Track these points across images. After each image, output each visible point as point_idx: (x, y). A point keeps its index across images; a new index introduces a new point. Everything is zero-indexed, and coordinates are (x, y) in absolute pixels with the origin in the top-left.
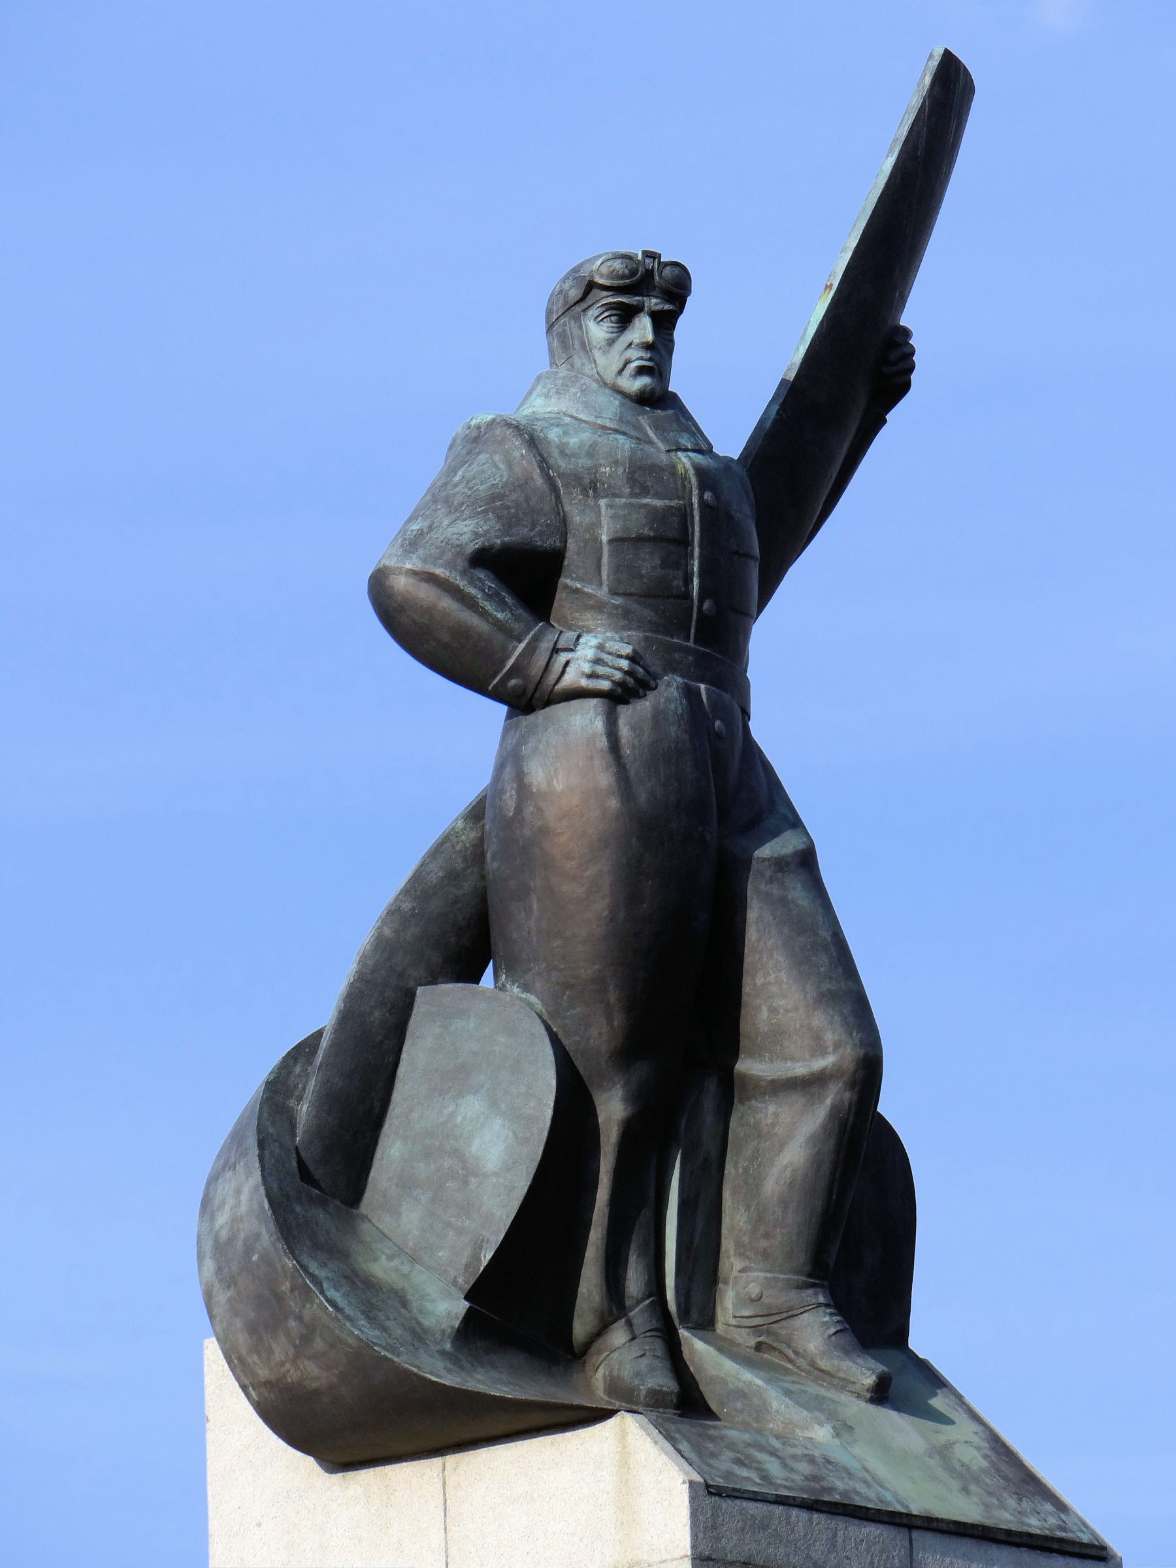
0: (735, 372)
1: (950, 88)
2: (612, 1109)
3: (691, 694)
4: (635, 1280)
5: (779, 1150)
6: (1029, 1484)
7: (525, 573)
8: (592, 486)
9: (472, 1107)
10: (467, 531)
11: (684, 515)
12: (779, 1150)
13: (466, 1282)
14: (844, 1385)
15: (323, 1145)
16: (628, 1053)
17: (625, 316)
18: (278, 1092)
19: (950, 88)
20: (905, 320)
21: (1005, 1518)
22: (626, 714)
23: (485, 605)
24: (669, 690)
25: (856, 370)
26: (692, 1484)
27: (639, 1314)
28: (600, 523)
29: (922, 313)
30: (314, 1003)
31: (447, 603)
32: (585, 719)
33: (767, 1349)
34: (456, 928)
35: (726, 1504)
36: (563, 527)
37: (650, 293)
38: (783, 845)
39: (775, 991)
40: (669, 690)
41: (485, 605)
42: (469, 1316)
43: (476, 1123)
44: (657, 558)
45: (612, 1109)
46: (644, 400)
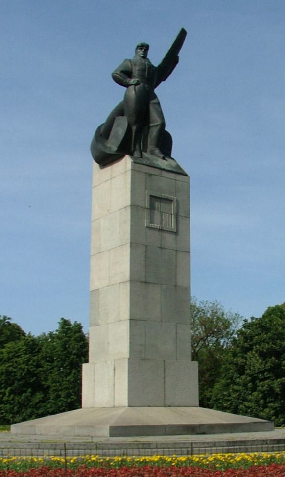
0: (156, 58)
1: (183, 35)
2: (134, 128)
3: (144, 86)
4: (137, 147)
5: (154, 132)
6: (180, 168)
7: (128, 73)
8: (135, 65)
9: (119, 128)
10: (121, 69)
11: (146, 68)
12: (154, 132)
13: (118, 145)
14: (159, 157)
15: (103, 133)
16: (136, 122)
17: (142, 49)
18: (99, 128)
19: (183, 35)
20: (179, 55)
21: (179, 171)
22: (137, 87)
23: (123, 77)
24: (142, 85)
25: (171, 60)
26: (132, 162)
27: (137, 151)
28: (136, 71)
29: (181, 54)
30: (103, 119)
31: (117, 76)
32: (132, 87)
33: (152, 153)
34: (120, 112)
35: (136, 164)
36: (132, 69)
37: (144, 48)
38: (154, 101)
39: (154, 115)
40: (142, 85)
41: (123, 77)
42: (117, 150)
43: (120, 130)
44: (146, 79)
45: (134, 128)
46: (143, 57)
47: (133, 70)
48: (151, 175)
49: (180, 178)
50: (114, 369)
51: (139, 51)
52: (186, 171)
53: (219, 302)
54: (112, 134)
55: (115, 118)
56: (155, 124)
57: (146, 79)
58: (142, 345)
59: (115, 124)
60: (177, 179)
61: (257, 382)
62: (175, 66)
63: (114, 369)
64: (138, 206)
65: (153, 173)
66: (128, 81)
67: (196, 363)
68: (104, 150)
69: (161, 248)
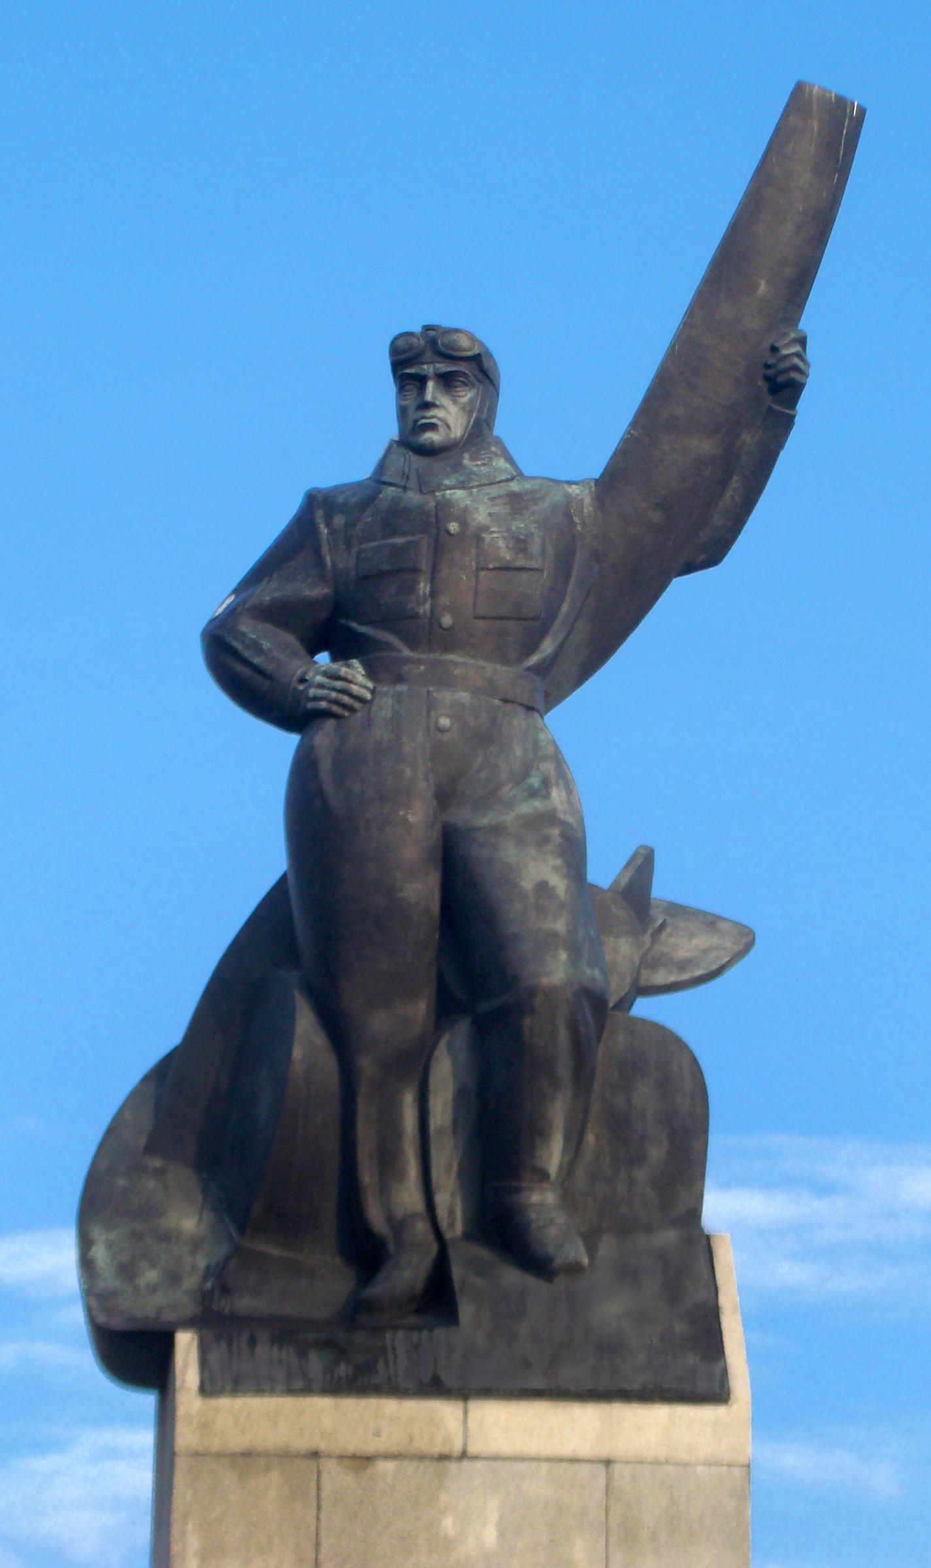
0: (564, 424)
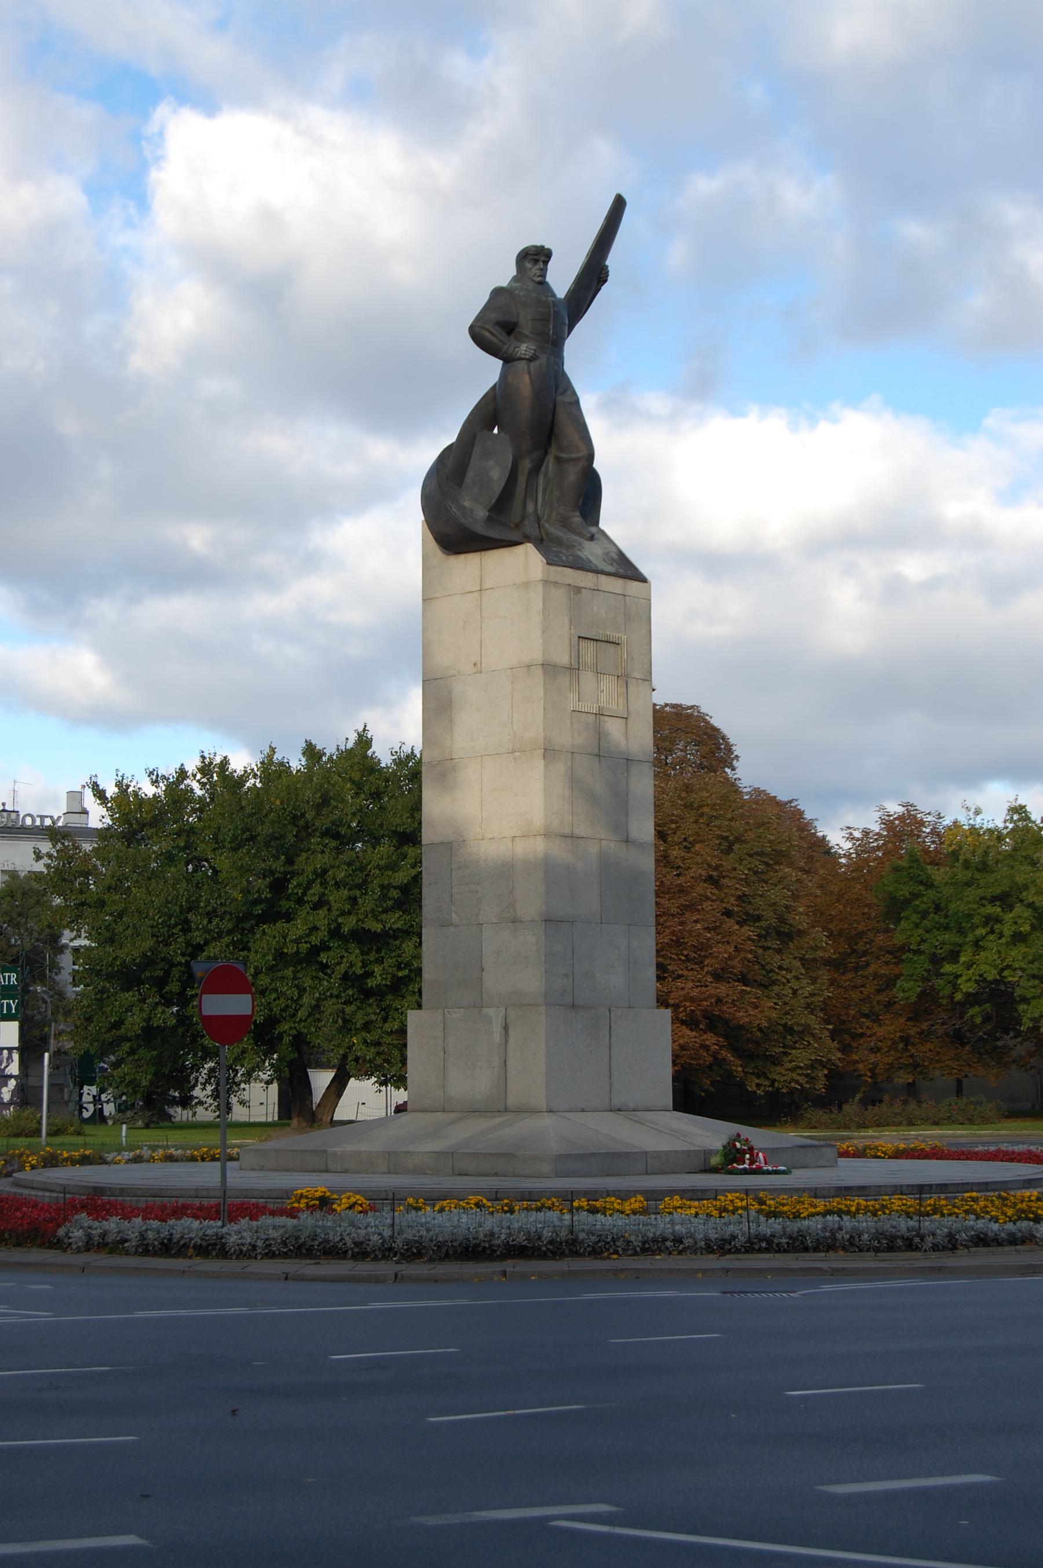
0: (561, 278)
1: (619, 205)
9: (491, 463)
19: (619, 205)
25: (593, 276)
29: (612, 261)
32: (522, 365)
47: (522, 320)
48: (578, 590)
49: (634, 586)
50: (506, 1028)
51: (529, 265)
52: (644, 569)
53: (128, 775)
54: (470, 474)
55: (475, 436)
56: (573, 456)
57: (529, 322)
58: (567, 975)
59: (477, 451)
60: (628, 593)
61: (958, 997)
62: (600, 289)
63: (506, 1028)
64: (554, 666)
65: (582, 585)
66: (512, 349)
67: (668, 1013)
68: (463, 520)
69: (598, 756)
